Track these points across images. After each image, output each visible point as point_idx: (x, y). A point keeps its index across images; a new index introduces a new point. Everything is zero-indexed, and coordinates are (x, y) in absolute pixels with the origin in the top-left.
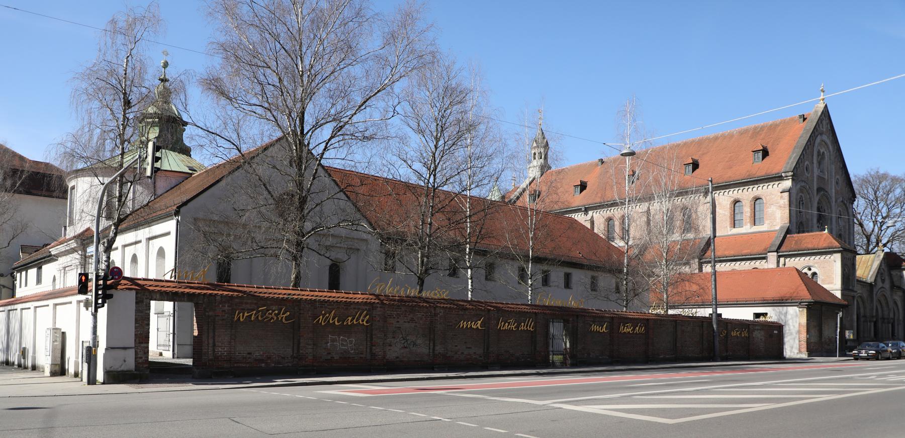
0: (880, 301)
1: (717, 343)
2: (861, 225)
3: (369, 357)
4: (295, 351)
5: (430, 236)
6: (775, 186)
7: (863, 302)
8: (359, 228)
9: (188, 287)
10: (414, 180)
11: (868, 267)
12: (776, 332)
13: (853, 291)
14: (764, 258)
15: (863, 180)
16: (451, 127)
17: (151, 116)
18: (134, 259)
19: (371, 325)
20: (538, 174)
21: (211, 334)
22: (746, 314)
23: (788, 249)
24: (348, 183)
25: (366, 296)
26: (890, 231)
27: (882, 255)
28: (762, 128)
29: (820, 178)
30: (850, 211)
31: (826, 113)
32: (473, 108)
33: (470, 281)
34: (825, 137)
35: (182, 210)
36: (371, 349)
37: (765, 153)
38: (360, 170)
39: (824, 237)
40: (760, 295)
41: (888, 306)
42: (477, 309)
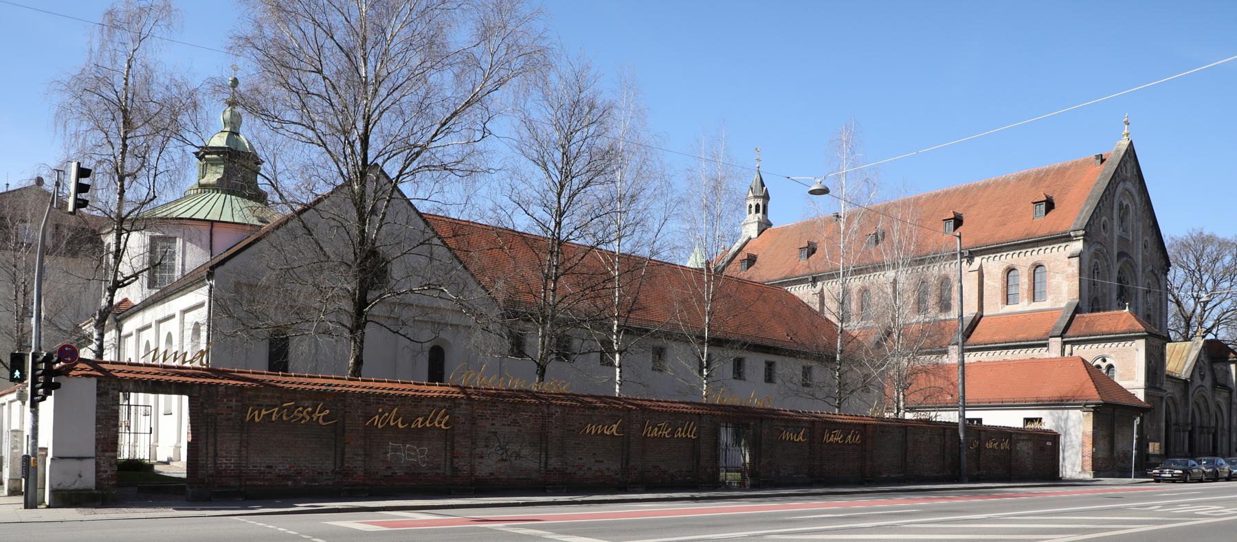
2: (1178, 303)
3: (448, 473)
7: (1175, 406)
8: (442, 295)
9: (177, 373)
10: (537, 231)
11: (1181, 358)
12: (1049, 444)
14: (1044, 345)
16: (580, 154)
17: (217, 150)
18: (169, 337)
19: (453, 429)
20: (754, 234)
21: (211, 440)
22: (1012, 419)
23: (1076, 333)
24: (455, 237)
26: (1216, 313)
27: (1202, 342)
28: (1047, 172)
30: (1163, 283)
31: (1131, 153)
32: (618, 130)
33: (618, 370)
34: (1129, 185)
35: (217, 271)
36: (452, 462)
37: (1050, 205)
38: (454, 215)
39: (1124, 318)
40: (1032, 395)
41: (1208, 411)
42: (612, 408)
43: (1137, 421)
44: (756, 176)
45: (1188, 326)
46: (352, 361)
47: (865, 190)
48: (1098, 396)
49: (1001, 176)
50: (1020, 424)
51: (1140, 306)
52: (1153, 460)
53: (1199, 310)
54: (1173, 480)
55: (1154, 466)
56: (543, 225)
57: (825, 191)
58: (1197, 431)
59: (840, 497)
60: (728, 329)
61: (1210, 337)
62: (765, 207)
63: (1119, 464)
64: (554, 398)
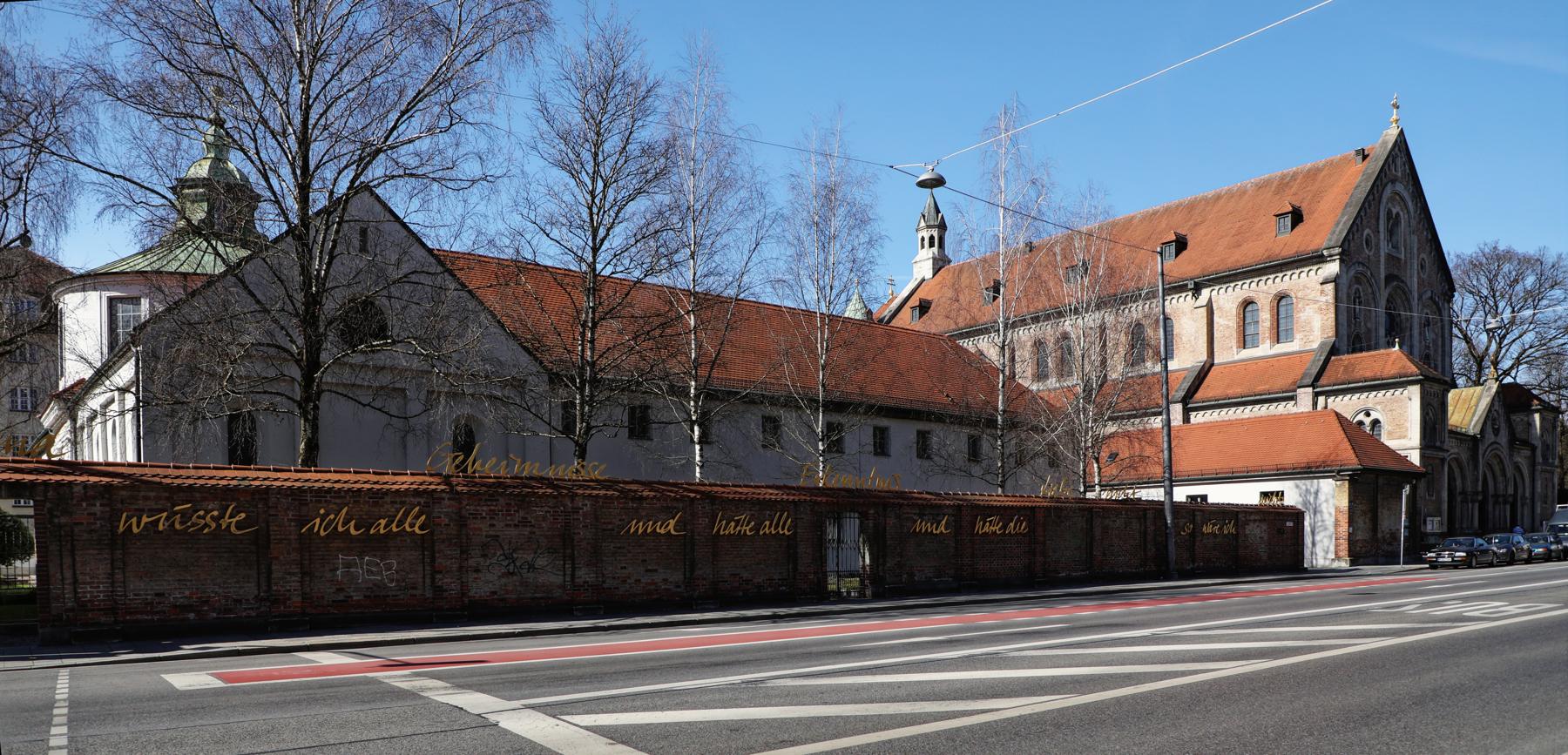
2: (1467, 339)
5: (593, 364)
6: (1312, 273)
7: (1461, 469)
9: (9, 469)
11: (1468, 407)
17: (195, 183)
19: (432, 533)
20: (929, 274)
21: (67, 561)
22: (1246, 494)
23: (1333, 380)
26: (1515, 350)
28: (1294, 176)
30: (1445, 313)
31: (1401, 145)
33: (697, 447)
34: (1400, 187)
36: (433, 579)
37: (1297, 217)
39: (1393, 358)
40: (1271, 462)
41: (1504, 474)
42: (676, 498)
43: (1406, 490)
45: (1480, 369)
48: (1355, 460)
50: (1254, 500)
52: (1432, 540)
53: (1494, 346)
54: (1455, 566)
60: (850, 389)
61: (1508, 380)
62: (941, 239)
63: (1385, 547)
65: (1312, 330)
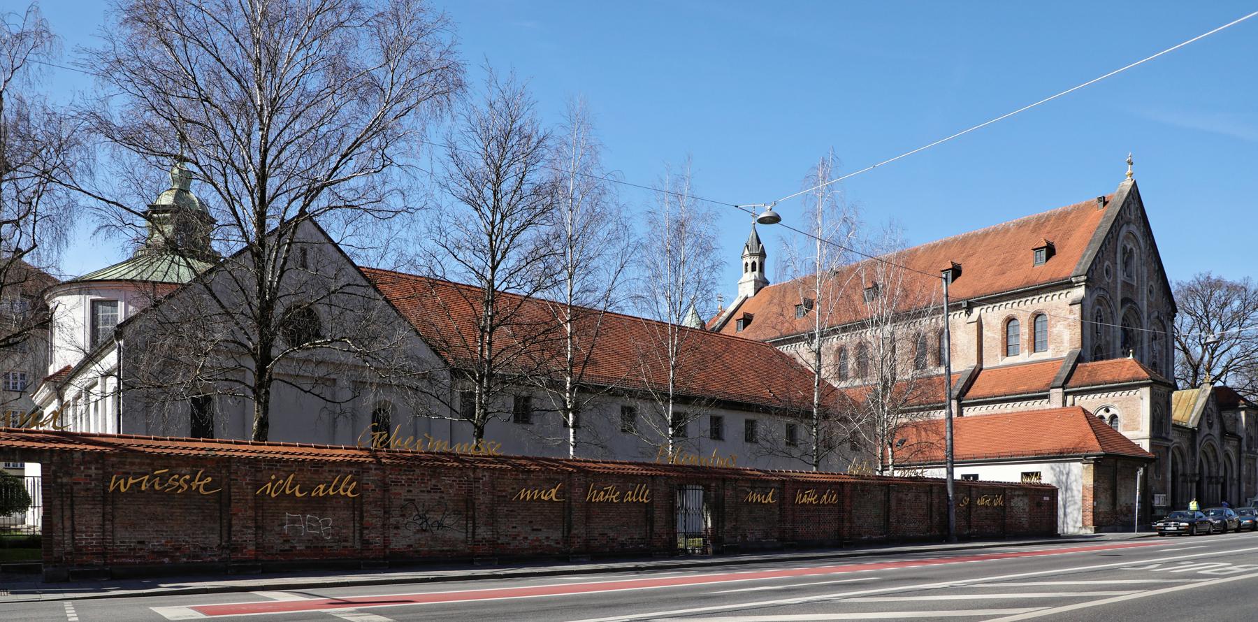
0: (1205, 453)
1: (953, 516)
4: (225, 539)
5: (490, 362)
6: (1063, 296)
7: (1182, 456)
9: (22, 438)
11: (1188, 405)
13: (1166, 439)
14: (1046, 397)
15: (1189, 289)
19: (361, 496)
20: (751, 293)
22: (1010, 474)
23: (1079, 382)
25: (352, 452)
26: (1224, 359)
27: (1209, 389)
28: (1048, 218)
29: (1127, 286)
30: (1169, 329)
31: (1134, 194)
33: (572, 431)
34: (1133, 228)
37: (1050, 251)
39: (1128, 365)
41: (1217, 460)
42: (554, 471)
43: (1141, 472)
44: (752, 233)
45: (1196, 374)
46: (255, 424)
47: (845, 230)
48: (1099, 448)
49: (1000, 223)
51: (1146, 354)
52: (1159, 513)
53: (1207, 357)
54: (1179, 533)
55: (1160, 518)
56: (481, 277)
57: (775, 219)
58: (1206, 481)
59: (798, 563)
61: (1219, 384)
63: (1122, 518)
64: (481, 461)
65: (1062, 342)
